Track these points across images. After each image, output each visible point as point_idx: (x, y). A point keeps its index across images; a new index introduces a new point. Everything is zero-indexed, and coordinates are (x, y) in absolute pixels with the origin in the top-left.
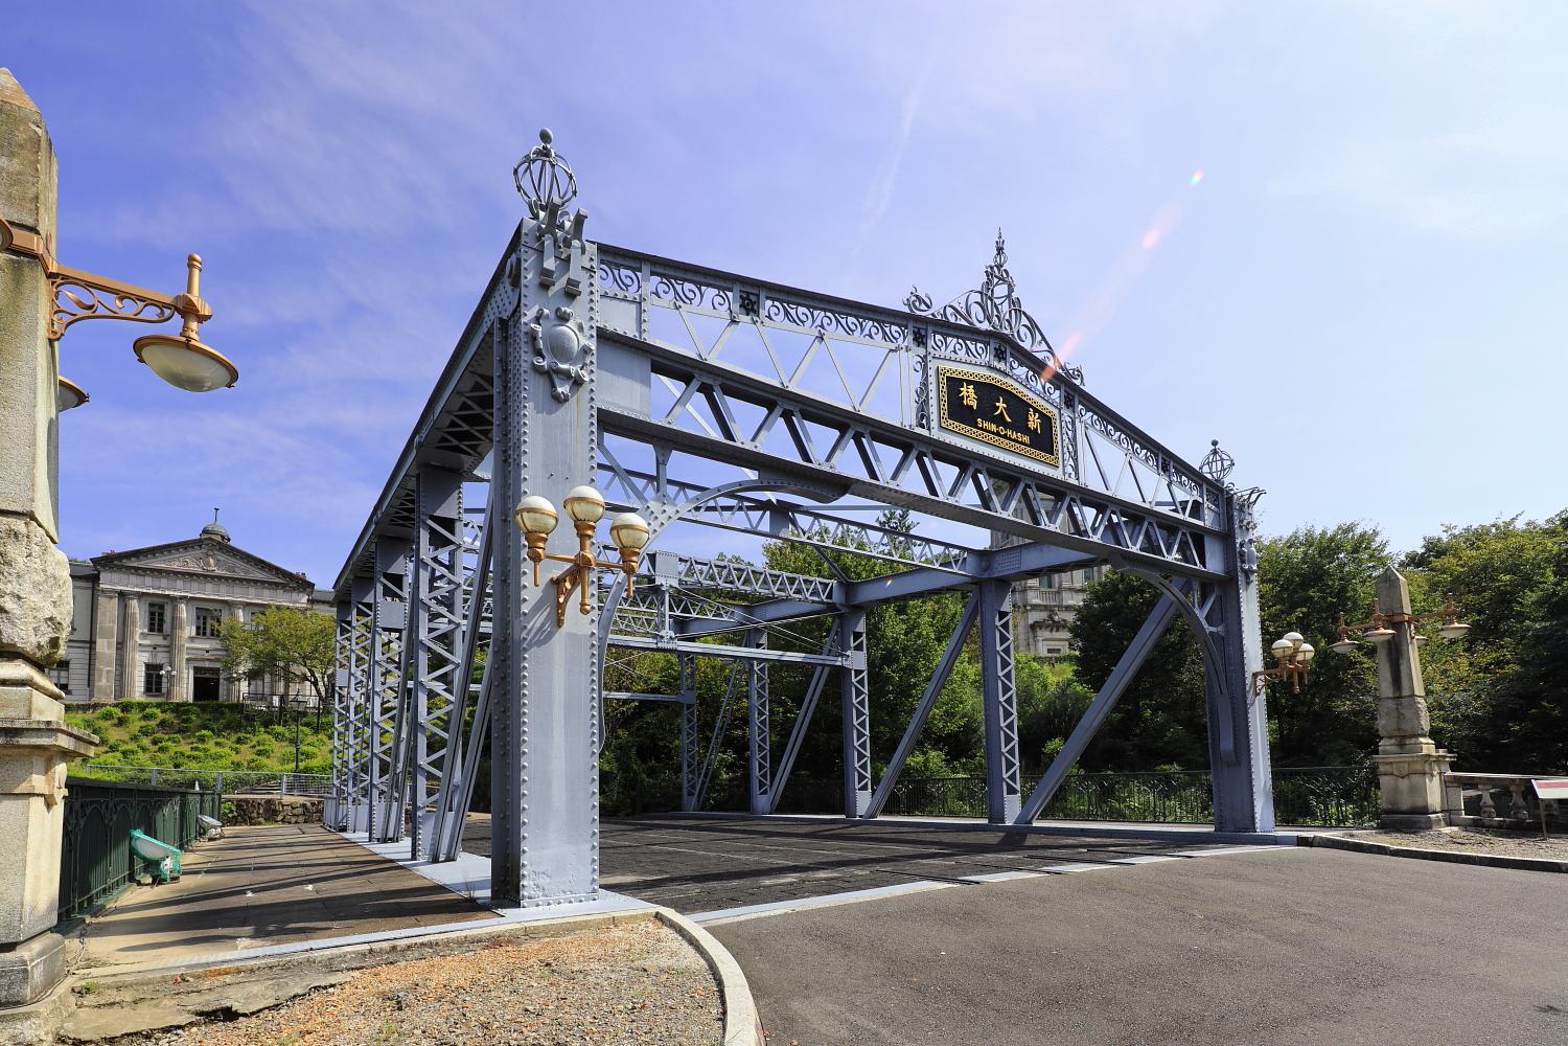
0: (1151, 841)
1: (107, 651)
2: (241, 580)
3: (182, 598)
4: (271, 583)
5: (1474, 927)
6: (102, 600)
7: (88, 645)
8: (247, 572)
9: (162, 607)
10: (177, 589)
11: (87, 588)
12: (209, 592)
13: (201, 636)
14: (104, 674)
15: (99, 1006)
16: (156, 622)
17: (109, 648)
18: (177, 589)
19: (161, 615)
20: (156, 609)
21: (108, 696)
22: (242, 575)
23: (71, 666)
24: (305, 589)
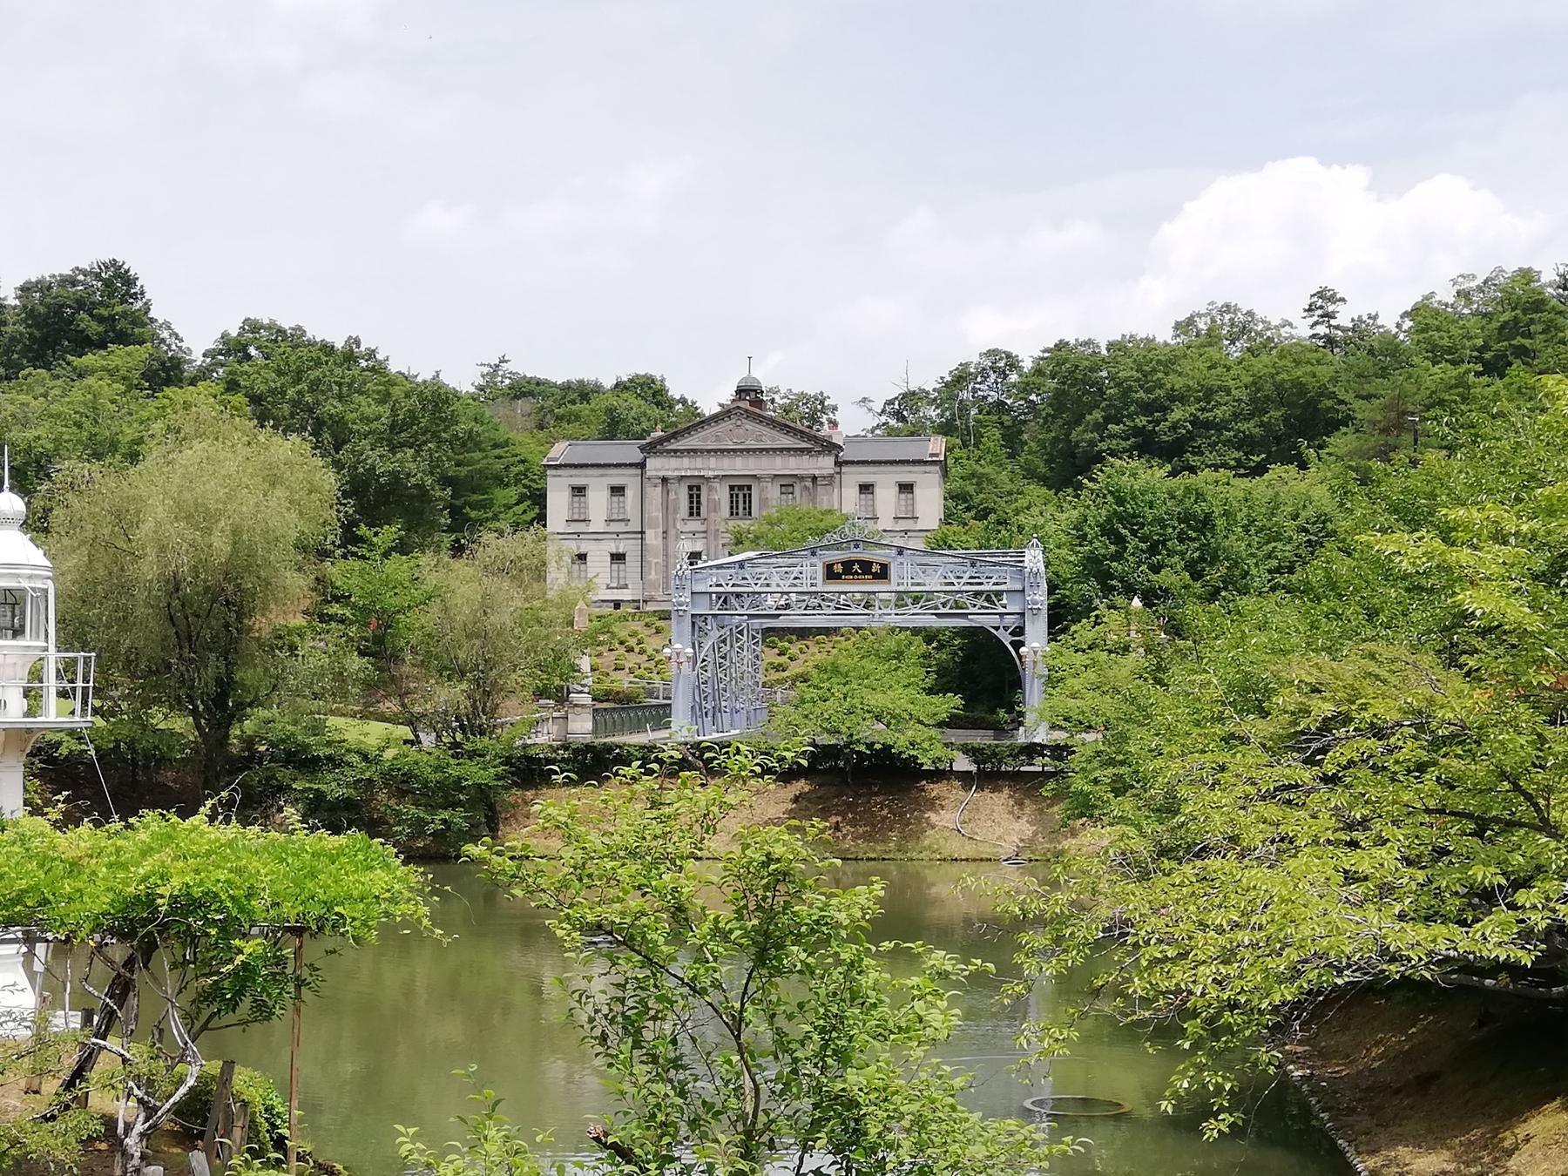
0: (173, 1023)
1: (654, 542)
2: (767, 450)
3: (716, 477)
4: (796, 450)
5: (1548, 444)
6: (649, 489)
7: (640, 536)
8: (774, 440)
9: (699, 488)
10: (711, 467)
11: (637, 475)
12: (740, 466)
13: (695, 517)
14: (653, 566)
15: (155, 979)
16: (695, 505)
17: (656, 538)
18: (711, 467)
19: (699, 496)
20: (695, 491)
21: (658, 589)
22: (768, 444)
23: (588, 558)
24: (830, 452)
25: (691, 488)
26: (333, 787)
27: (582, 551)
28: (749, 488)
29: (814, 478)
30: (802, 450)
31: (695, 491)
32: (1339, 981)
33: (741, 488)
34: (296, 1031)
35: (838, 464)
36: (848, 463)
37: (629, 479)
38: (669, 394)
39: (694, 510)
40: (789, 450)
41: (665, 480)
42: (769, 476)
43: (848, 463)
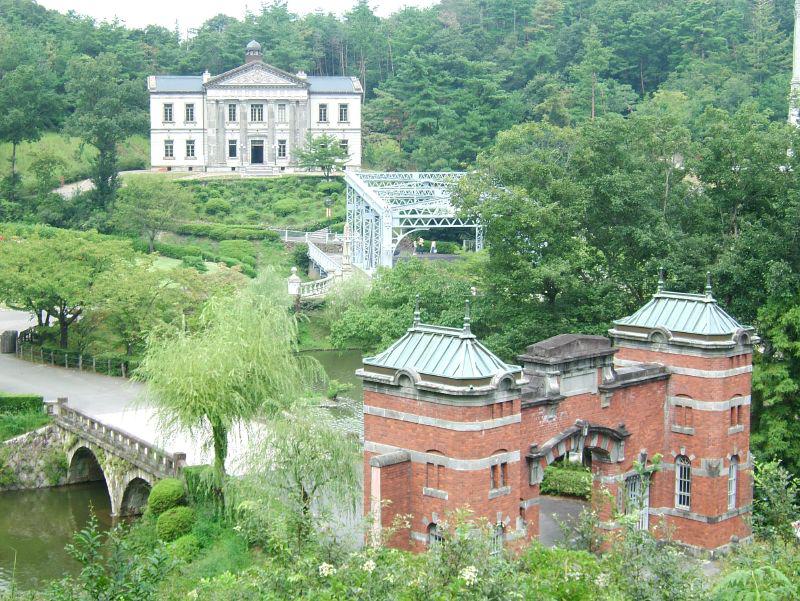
9: (234, 106)
10: (243, 95)
12: (258, 95)
18: (243, 95)
20: (232, 108)
22: (264, 82)
25: (230, 106)
26: (222, 442)
27: (171, 139)
28: (262, 106)
29: (298, 102)
30: (292, 87)
31: (232, 108)
32: (16, 110)
33: (257, 106)
34: (446, 388)
35: (310, 93)
36: (314, 93)
37: (196, 100)
38: (97, 26)
39: (232, 117)
40: (284, 87)
41: (217, 102)
42: (245, 100)
43: (314, 93)
